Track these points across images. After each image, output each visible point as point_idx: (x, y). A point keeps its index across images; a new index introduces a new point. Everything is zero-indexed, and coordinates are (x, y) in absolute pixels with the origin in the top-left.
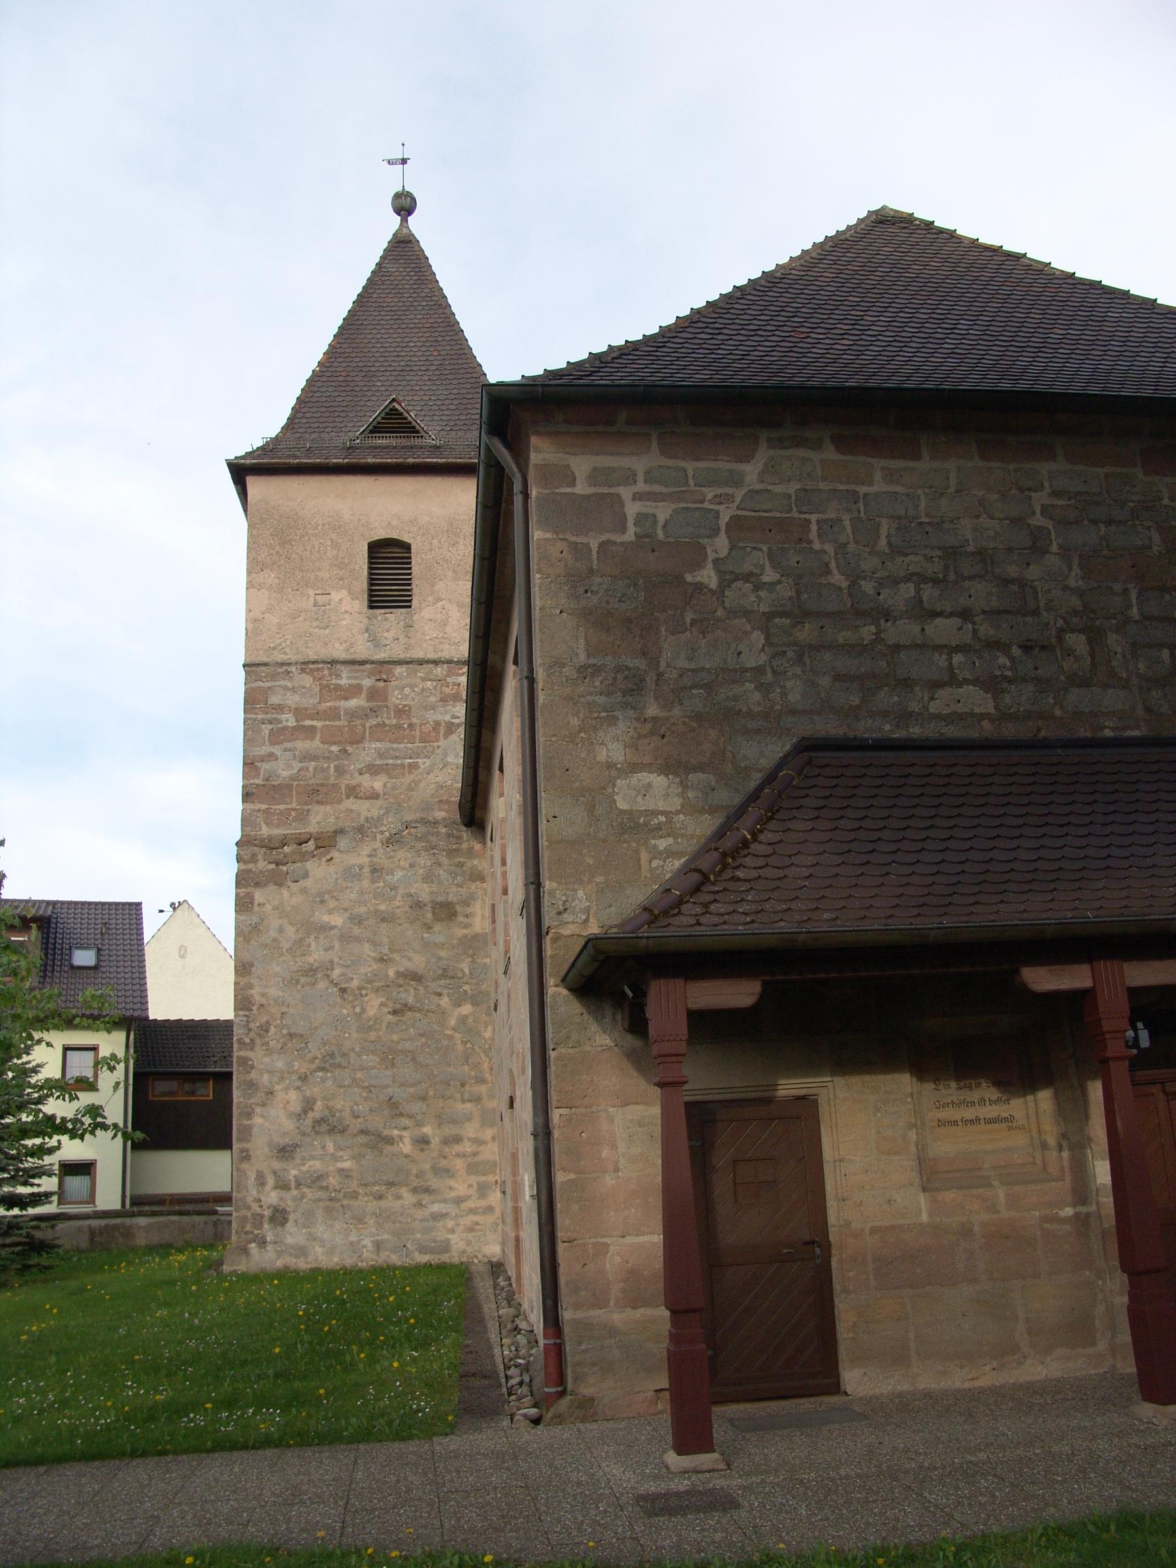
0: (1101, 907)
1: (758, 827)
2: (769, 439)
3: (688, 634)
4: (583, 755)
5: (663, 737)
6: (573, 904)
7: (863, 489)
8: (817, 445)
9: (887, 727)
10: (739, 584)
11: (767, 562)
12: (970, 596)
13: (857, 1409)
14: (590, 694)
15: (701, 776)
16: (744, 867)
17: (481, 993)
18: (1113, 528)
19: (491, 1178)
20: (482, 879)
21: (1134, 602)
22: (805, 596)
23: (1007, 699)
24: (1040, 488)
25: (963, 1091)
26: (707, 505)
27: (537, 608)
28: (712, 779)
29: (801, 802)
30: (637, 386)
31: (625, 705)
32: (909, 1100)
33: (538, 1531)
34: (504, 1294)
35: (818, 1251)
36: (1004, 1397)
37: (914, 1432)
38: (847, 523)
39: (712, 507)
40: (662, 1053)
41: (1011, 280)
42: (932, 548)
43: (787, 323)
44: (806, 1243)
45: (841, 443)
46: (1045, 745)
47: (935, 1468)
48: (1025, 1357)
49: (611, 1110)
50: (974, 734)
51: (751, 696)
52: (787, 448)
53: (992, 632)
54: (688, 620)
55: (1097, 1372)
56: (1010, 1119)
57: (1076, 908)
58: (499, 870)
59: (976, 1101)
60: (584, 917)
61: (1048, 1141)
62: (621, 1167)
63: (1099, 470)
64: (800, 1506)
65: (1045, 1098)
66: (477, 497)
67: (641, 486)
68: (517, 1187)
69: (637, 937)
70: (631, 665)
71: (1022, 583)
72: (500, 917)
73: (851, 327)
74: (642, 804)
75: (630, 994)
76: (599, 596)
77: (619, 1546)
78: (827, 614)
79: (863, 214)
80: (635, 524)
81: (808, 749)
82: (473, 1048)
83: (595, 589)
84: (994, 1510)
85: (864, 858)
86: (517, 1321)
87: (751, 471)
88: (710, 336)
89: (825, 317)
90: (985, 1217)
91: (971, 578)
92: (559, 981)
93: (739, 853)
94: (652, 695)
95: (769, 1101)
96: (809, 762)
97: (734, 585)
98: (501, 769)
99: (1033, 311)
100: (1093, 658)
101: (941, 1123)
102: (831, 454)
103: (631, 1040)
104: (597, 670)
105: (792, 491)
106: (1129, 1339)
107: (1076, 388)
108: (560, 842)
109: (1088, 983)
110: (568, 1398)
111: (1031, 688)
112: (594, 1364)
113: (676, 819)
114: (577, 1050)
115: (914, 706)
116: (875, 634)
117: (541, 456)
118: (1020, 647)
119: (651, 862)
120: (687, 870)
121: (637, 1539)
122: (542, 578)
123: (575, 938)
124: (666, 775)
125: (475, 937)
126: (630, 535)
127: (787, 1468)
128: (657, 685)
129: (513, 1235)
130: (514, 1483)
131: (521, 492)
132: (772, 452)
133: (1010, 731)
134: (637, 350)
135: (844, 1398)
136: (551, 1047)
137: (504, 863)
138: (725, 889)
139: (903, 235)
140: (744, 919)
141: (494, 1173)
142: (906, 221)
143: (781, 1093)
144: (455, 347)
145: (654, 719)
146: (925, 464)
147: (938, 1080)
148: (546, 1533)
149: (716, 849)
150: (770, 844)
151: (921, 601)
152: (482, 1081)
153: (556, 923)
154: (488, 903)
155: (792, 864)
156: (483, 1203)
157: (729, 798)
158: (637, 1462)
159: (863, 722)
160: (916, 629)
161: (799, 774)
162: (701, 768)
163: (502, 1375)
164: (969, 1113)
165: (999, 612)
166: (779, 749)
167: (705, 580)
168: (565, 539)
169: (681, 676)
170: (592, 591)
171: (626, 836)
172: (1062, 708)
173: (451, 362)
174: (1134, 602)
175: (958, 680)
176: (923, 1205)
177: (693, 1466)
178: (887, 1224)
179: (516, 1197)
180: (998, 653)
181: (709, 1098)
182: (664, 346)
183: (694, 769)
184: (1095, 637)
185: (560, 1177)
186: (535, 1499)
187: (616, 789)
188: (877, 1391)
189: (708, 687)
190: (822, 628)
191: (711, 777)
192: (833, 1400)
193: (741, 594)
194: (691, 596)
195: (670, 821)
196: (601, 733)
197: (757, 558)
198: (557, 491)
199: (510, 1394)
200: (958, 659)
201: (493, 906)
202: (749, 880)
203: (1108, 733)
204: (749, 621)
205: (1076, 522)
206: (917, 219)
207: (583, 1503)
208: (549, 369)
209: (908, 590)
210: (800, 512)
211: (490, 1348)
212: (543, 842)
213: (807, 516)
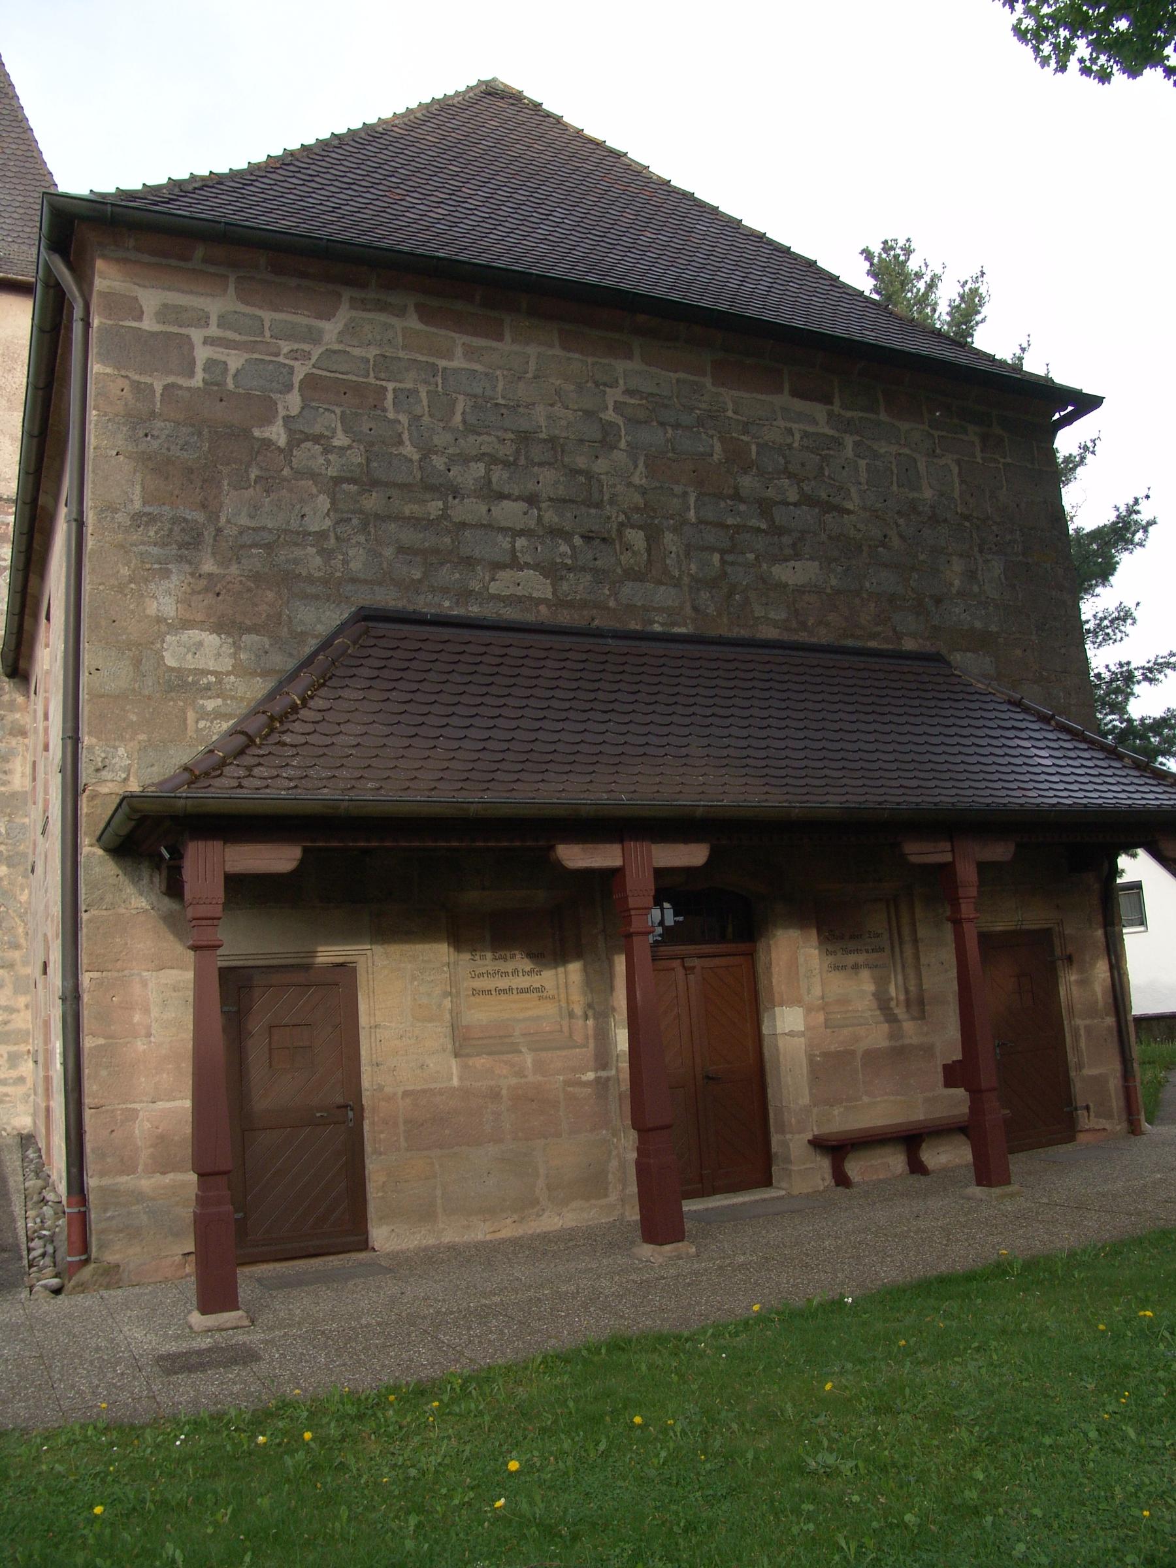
0: (635, 791)
1: (309, 693)
2: (352, 299)
3: (251, 490)
4: (132, 607)
5: (218, 594)
6: (113, 762)
7: (442, 363)
8: (401, 312)
9: (447, 604)
10: (309, 444)
11: (339, 425)
12: (538, 482)
13: (383, 1263)
14: (143, 543)
15: (255, 638)
16: (292, 732)
17: (17, 853)
18: (680, 432)
19: (23, 1048)
20: (23, 733)
21: (692, 506)
22: (375, 464)
23: (565, 586)
24: (613, 384)
25: (497, 962)
26: (281, 359)
27: (92, 447)
28: (266, 642)
29: (354, 671)
30: (217, 222)
31: (180, 559)
32: (445, 969)
33: (49, 1398)
34: (32, 1167)
35: (351, 1114)
36: (522, 1246)
37: (435, 1282)
38: (423, 395)
39: (287, 362)
40: (198, 916)
41: (610, 176)
42: (506, 430)
43: (383, 182)
44: (339, 1107)
45: (426, 315)
46: (599, 634)
47: (452, 1313)
48: (543, 1210)
49: (145, 974)
50: (530, 617)
51: (312, 561)
52: (369, 310)
53: (556, 519)
54: (253, 476)
55: (607, 1220)
56: (541, 989)
57: (612, 791)
58: (41, 725)
59: (510, 971)
60: (124, 776)
61: (576, 1011)
62: (153, 1032)
63: (672, 374)
64: (320, 1355)
65: (574, 969)
66: (33, 319)
67: (213, 331)
68: (48, 1053)
69: (175, 797)
70: (189, 517)
71: (589, 475)
72: (40, 776)
73: (448, 197)
74: (191, 663)
75: (167, 856)
76: (160, 441)
77: (135, 1405)
78: (396, 485)
79: (473, 83)
80: (204, 370)
81: (366, 618)
82: (7, 912)
83: (156, 433)
84: (501, 1345)
85: (413, 731)
86: (45, 1193)
87: (331, 329)
88: (301, 182)
89: (424, 181)
90: (513, 1081)
91: (540, 464)
92: (94, 841)
93: (287, 718)
94: (209, 551)
95: (307, 968)
96: (367, 632)
97: (303, 445)
98: (48, 618)
99: (628, 210)
100: (649, 555)
101: (475, 992)
102: (413, 322)
103: (168, 904)
104: (152, 519)
105: (371, 357)
106: (636, 1190)
107: (659, 292)
108: (103, 696)
109: (618, 863)
110: (92, 1266)
111: (589, 577)
112: (121, 1231)
113: (226, 680)
114: (110, 912)
115: (475, 585)
116: (442, 510)
117: (107, 283)
118: (582, 537)
119: (197, 722)
120: (233, 732)
121: (154, 1397)
122: (99, 415)
123: (114, 796)
124: (219, 635)
125: (14, 795)
126: (198, 380)
127: (311, 1321)
128: (215, 540)
129: (43, 1105)
130: (27, 1354)
131: (82, 320)
132: (354, 313)
133: (565, 618)
134: (222, 184)
135: (372, 1254)
136: (84, 908)
137: (46, 717)
138: (270, 753)
139: (512, 111)
140: (287, 783)
141: (26, 1042)
142: (515, 98)
143: (319, 960)
144: (22, 147)
145: (210, 575)
146: (507, 346)
147: (475, 950)
148: (58, 1400)
149: (264, 712)
150: (319, 711)
151: (490, 482)
152: (17, 947)
153: (94, 780)
154: (30, 758)
155: (341, 732)
156: (14, 1074)
157: (284, 662)
158: (159, 1324)
159: (422, 597)
160: (483, 509)
161: (355, 643)
162: (254, 629)
163: (24, 1247)
164: (503, 983)
165: (564, 501)
166: (337, 617)
167: (274, 437)
168: (127, 377)
169: (241, 533)
170: (152, 436)
171: (173, 694)
172: (616, 600)
173: (17, 163)
174: (692, 506)
175: (519, 563)
176: (455, 1071)
177: (217, 1324)
178: (419, 1088)
179: (47, 1066)
180: (560, 541)
181: (250, 963)
182: (251, 185)
183: (249, 630)
184: (653, 536)
185: (88, 1043)
186: (49, 1368)
187: (165, 646)
188: (404, 1246)
189: (269, 547)
190: (389, 498)
191: (266, 639)
192: (362, 1256)
193: (309, 455)
194: (258, 452)
195: (220, 682)
196: (152, 586)
197: (328, 421)
198: (121, 323)
199: (31, 1266)
200: (521, 542)
201: (34, 763)
202: (296, 746)
203: (657, 628)
204: (316, 483)
205: (646, 422)
206: (525, 98)
207: (100, 1367)
208: (121, 188)
209: (478, 469)
210: (377, 379)
211: (14, 1221)
212: (84, 696)
213: (384, 383)
